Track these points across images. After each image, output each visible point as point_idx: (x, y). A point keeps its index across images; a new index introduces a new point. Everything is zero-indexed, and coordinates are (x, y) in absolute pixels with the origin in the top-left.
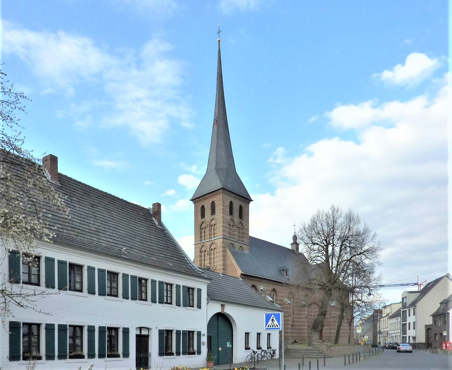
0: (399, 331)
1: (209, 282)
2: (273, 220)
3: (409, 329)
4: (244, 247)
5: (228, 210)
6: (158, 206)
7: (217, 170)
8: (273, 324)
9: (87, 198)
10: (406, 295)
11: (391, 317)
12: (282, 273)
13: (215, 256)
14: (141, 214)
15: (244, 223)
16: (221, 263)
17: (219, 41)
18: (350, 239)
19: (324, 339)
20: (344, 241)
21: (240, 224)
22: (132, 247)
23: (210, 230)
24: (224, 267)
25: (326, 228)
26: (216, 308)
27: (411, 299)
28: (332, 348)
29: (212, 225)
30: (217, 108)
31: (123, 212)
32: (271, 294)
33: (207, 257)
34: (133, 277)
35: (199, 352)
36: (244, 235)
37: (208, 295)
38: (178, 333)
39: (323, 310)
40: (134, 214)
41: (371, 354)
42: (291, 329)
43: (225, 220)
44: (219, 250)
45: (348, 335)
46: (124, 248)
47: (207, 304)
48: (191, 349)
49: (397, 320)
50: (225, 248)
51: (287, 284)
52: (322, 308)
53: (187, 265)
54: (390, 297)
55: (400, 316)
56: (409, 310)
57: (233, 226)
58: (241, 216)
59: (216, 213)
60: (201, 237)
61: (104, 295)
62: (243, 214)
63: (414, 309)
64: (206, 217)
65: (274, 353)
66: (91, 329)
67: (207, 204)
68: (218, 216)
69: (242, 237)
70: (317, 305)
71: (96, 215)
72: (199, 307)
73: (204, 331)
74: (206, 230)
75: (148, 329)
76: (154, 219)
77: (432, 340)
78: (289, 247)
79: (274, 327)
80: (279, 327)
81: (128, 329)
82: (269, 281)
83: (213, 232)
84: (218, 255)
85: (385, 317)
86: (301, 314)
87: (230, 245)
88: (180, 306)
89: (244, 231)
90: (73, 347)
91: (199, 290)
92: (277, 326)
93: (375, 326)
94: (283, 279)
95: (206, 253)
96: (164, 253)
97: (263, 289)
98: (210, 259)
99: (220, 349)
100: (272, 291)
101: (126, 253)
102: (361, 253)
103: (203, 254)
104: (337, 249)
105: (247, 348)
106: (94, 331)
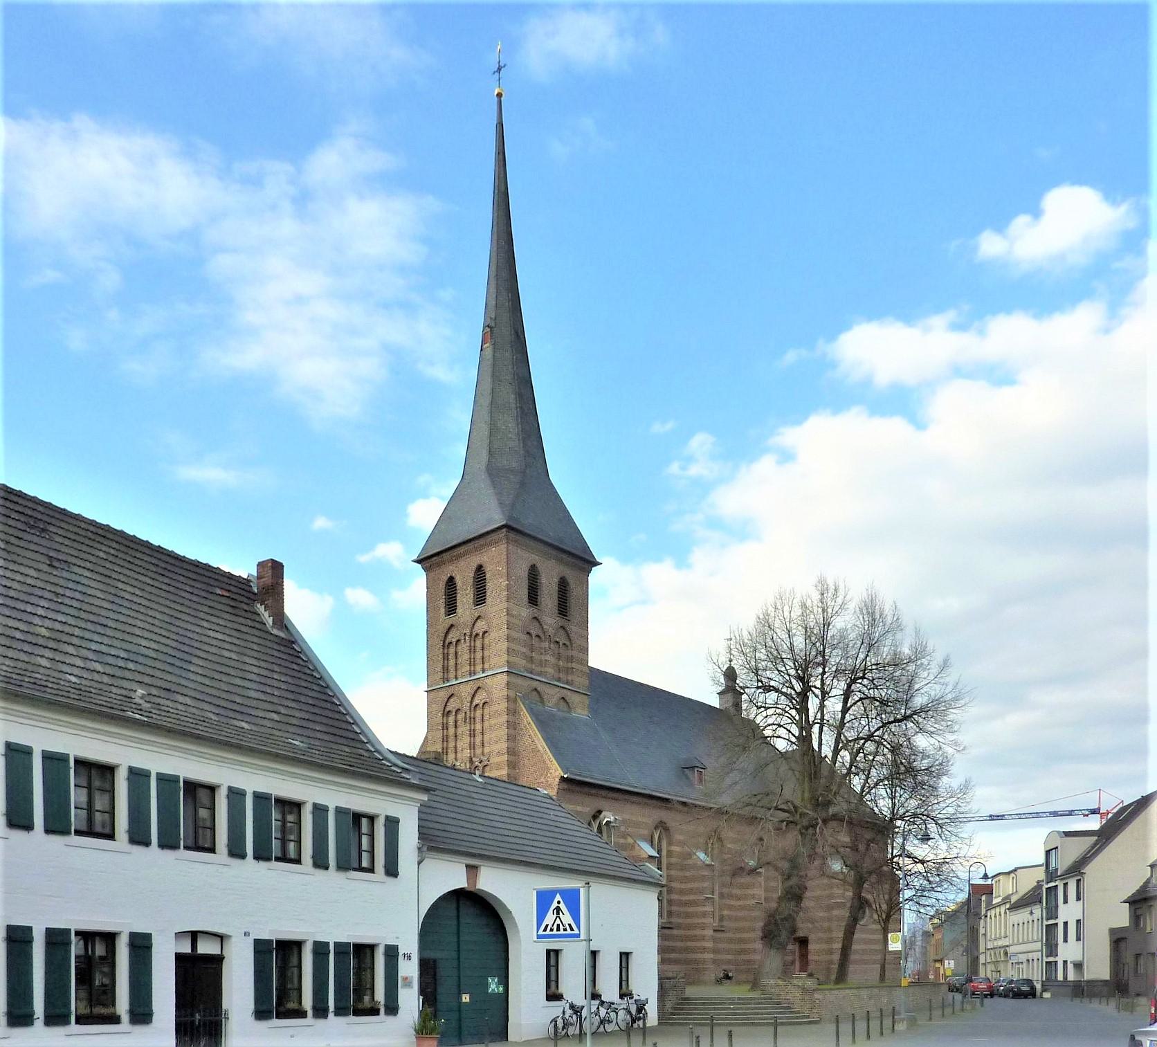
0: (1038, 946)
1: (425, 797)
2: (659, 626)
3: (1065, 940)
4: (575, 699)
5: (524, 592)
6: (274, 569)
7: (493, 472)
8: (558, 921)
9: (35, 539)
10: (1057, 842)
11: (1016, 907)
12: (687, 778)
13: (486, 724)
14: (219, 591)
15: (573, 628)
16: (504, 746)
17: (499, 95)
18: (875, 674)
19: (811, 967)
20: (853, 681)
21: (561, 632)
22: (173, 688)
23: (472, 650)
24: (512, 758)
25: (799, 642)
26: (448, 876)
27: (1071, 853)
28: (816, 996)
29: (477, 635)
30: (493, 290)
31: (156, 584)
32: (652, 837)
33: (464, 729)
34: (167, 781)
35: (392, 1009)
36: (574, 665)
37: (423, 836)
38: (320, 950)
39: (794, 881)
40: (196, 592)
41: (948, 1011)
42: (715, 940)
43: (513, 620)
44: (497, 708)
45: (879, 957)
46: (140, 692)
47: (419, 863)
48: (367, 998)
49: (1032, 913)
50: (515, 701)
51: (684, 804)
52: (789, 877)
53: (359, 745)
54: (1005, 850)
55: (1041, 902)
56: (1065, 885)
57: (538, 636)
58: (563, 608)
59: (489, 600)
60: (445, 670)
61: (65, 832)
62: (570, 605)
63: (1078, 881)
64: (459, 610)
65: (640, 1009)
66: (139, 942)
67: (463, 574)
68: (495, 608)
69: (569, 671)
70: (776, 868)
71: (60, 591)
72: (392, 870)
73: (409, 944)
74: (459, 648)
75: (221, 938)
76: (261, 608)
77: (1128, 974)
78: (714, 702)
79: (562, 932)
80: (576, 931)
81: (147, 938)
82: (645, 800)
83: (479, 655)
84: (493, 722)
85: (999, 905)
86: (746, 897)
87: (527, 692)
88: (327, 868)
89: (575, 653)
90: (283, 995)
91: (392, 824)
92: (572, 929)
93: (973, 935)
94: (692, 794)
95: (460, 716)
96: (283, 711)
97: (612, 819)
98: (472, 734)
99: (466, 998)
100: (656, 828)
101: (146, 706)
102: (906, 718)
103: (451, 719)
104: (834, 705)
105: (554, 996)
106: (29, 941)
